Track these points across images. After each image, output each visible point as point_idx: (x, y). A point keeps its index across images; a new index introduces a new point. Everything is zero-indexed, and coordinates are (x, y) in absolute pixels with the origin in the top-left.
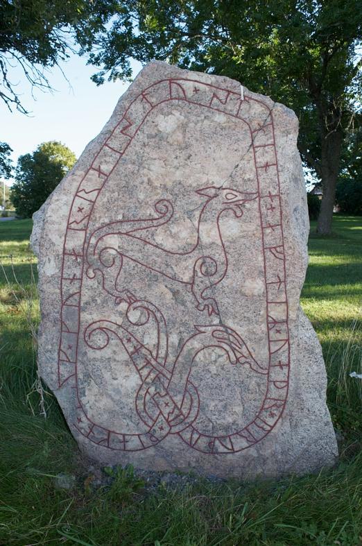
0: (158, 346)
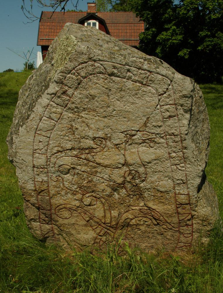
0: (105, 216)
